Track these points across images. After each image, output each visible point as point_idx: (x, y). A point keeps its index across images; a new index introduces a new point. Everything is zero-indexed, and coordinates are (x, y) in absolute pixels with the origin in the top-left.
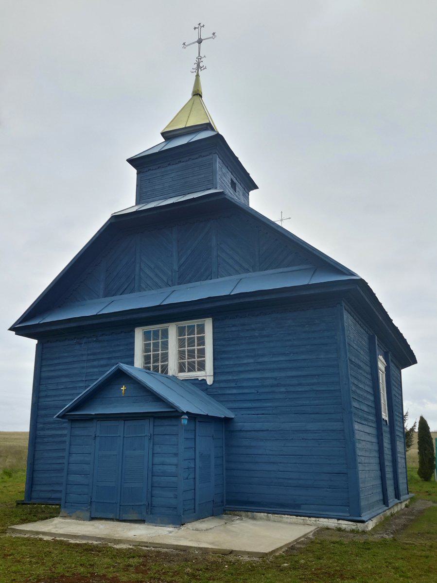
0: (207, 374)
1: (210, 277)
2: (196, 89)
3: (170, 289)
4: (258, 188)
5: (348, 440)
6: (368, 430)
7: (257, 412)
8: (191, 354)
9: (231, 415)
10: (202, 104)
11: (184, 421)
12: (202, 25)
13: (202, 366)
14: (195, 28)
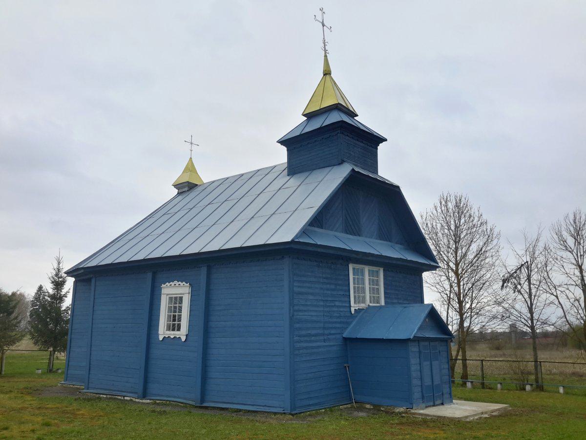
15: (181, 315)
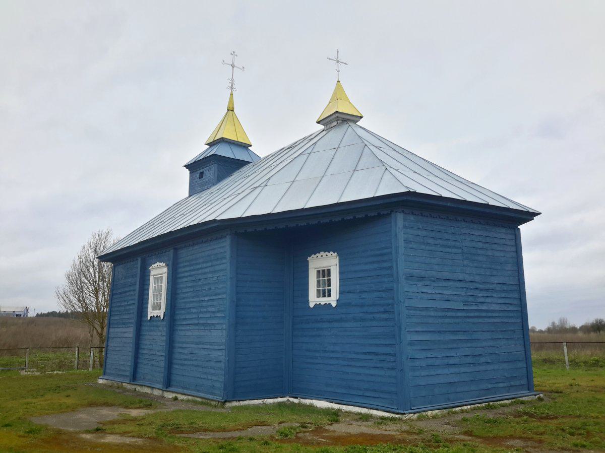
12: (232, 53)
15: (330, 279)
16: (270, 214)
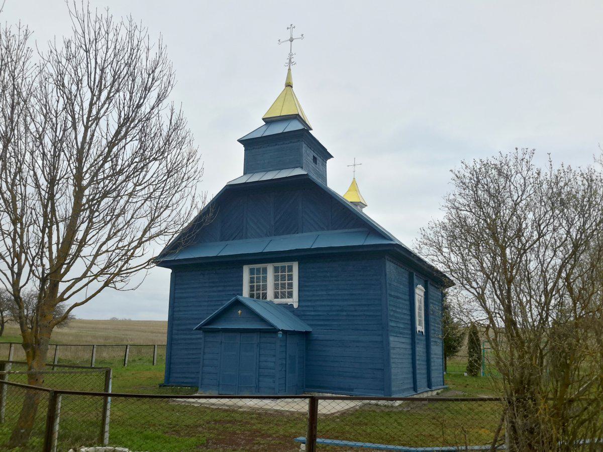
0: (294, 301)
1: (297, 232)
2: (288, 82)
3: (270, 239)
4: (332, 157)
5: (384, 348)
6: (403, 340)
7: (328, 328)
8: (283, 286)
9: (309, 329)
10: (293, 94)
11: (280, 335)
12: (293, 26)
13: (290, 295)
14: (288, 28)
16: (245, 183)
